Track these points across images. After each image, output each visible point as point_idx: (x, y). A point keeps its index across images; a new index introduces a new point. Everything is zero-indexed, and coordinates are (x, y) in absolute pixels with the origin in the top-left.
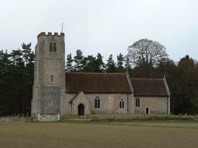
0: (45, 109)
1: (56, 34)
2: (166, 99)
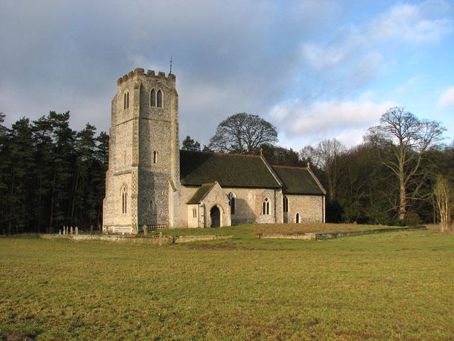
0: (143, 215)
1: (162, 75)
2: (320, 198)
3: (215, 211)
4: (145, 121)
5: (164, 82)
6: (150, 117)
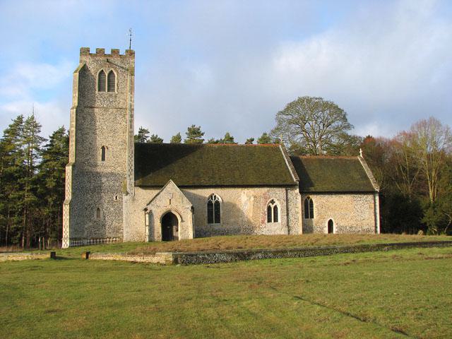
2: (370, 197)
3: (169, 220)
4: (90, 110)
5: (117, 61)
6: (98, 104)
